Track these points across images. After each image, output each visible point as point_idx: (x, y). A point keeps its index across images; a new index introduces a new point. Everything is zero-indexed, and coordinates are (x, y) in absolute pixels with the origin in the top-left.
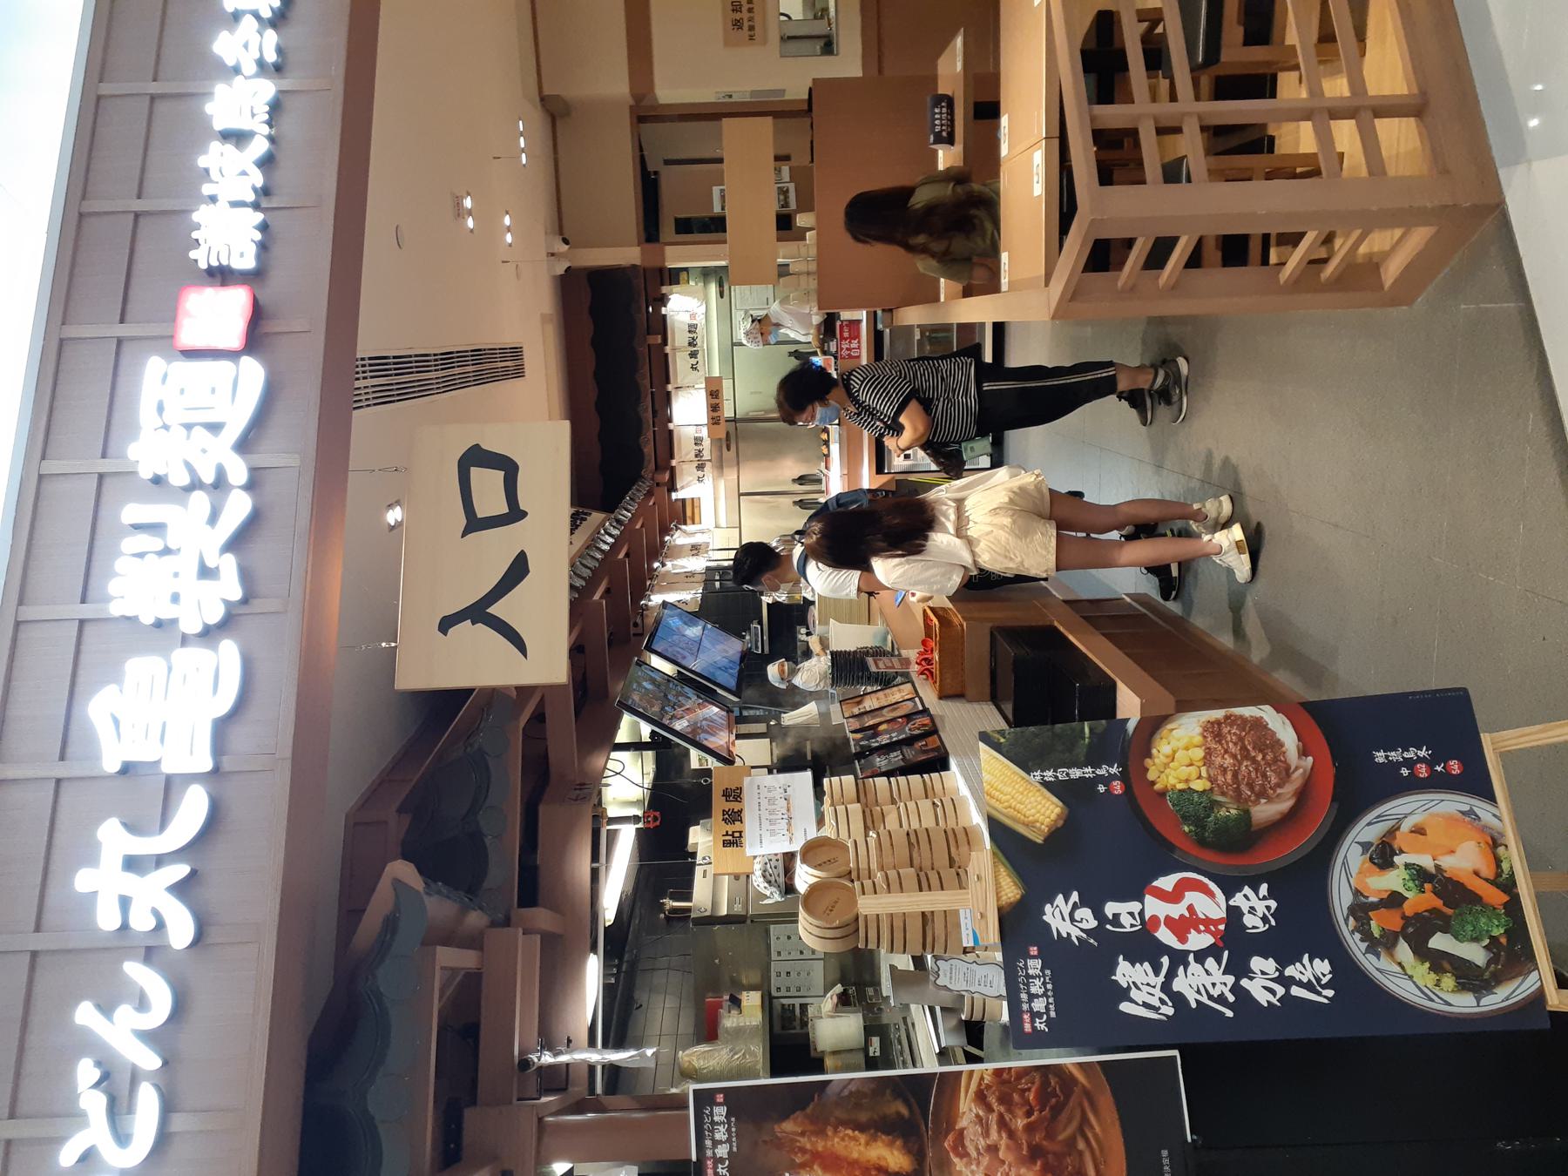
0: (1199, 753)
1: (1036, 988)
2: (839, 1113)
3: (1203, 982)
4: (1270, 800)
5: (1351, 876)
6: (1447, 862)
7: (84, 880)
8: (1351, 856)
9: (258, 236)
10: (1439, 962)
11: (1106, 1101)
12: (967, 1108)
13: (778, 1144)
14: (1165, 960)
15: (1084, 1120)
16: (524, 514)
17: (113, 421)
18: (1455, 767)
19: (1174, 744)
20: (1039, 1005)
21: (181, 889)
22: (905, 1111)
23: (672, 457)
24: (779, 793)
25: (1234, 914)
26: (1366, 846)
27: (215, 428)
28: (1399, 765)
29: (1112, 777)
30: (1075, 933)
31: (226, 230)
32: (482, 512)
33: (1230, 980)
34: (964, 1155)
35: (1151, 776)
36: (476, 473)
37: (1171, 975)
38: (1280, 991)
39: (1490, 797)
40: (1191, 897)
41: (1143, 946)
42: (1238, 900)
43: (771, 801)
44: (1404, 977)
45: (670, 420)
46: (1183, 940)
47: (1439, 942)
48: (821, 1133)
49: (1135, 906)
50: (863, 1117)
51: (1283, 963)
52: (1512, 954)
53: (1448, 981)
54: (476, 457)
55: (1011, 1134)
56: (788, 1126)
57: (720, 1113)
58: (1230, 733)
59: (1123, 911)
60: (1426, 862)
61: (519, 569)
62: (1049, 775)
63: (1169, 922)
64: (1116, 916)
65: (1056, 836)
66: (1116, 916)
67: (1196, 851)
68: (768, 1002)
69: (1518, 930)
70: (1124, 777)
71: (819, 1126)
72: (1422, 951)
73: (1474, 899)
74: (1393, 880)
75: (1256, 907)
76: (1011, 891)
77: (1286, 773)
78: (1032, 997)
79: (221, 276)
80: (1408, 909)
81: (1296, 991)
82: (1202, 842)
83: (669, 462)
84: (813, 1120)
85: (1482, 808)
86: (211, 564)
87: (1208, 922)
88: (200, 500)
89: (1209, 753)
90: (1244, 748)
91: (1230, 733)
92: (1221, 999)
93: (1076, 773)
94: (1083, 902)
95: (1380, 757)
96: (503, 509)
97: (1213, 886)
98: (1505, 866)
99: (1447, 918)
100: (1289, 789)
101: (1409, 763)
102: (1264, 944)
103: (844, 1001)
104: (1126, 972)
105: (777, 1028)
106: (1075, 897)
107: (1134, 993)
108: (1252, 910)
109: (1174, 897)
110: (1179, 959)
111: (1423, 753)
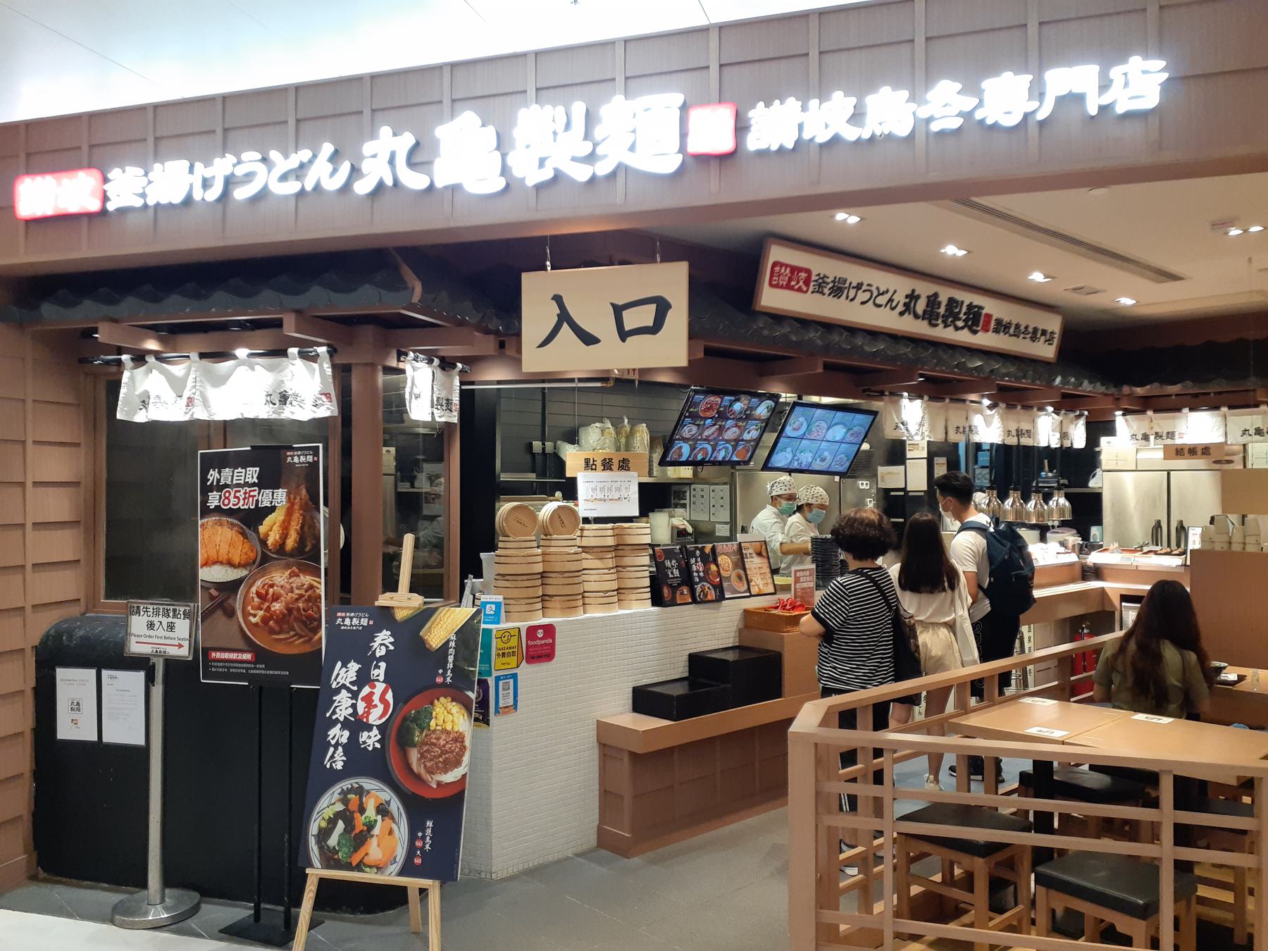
0: (449, 728)
1: (355, 621)
2: (308, 517)
3: (343, 705)
4: (419, 760)
5: (377, 792)
6: (374, 841)
7: (385, 131)
8: (386, 795)
9: (774, 148)
10: (332, 822)
11: (307, 649)
12: (307, 579)
13: (298, 486)
14: (355, 688)
15: (301, 637)
16: (623, 340)
17: (633, 82)
18: (418, 861)
19: (456, 715)
20: (347, 621)
21: (380, 186)
22: (307, 549)
23: (1156, 411)
24: (624, 493)
25: (369, 728)
26: (388, 803)
27: (632, 148)
28: (424, 832)
29: (445, 679)
30: (375, 645)
31: (777, 125)
32: (626, 314)
33: (342, 719)
34: (291, 576)
35: (442, 699)
36: (652, 308)
37: (349, 690)
38: (333, 742)
39: (401, 873)
40: (381, 707)
41: (363, 678)
42: (375, 731)
43: (618, 489)
44: (328, 804)
45: (1191, 409)
46: (363, 699)
47: (341, 825)
48: (301, 508)
49: (382, 678)
50: (306, 529)
51: (344, 746)
52: (330, 859)
53: (324, 824)
54: (663, 307)
55: (297, 600)
56: (304, 492)
57: (310, 458)
58: (456, 747)
59: (379, 672)
60: (376, 831)
61: (588, 339)
62: (452, 644)
63: (372, 694)
64: (379, 667)
65: (422, 643)
66: (379, 667)
67: (402, 713)
68: (686, 483)
69: (338, 865)
70: (444, 685)
71: (305, 508)
72: (338, 815)
73: (356, 849)
74: (371, 812)
75: (370, 739)
76: (400, 615)
77: (431, 772)
78: (351, 618)
79: (741, 128)
80: (357, 815)
81: (332, 749)
82: (405, 719)
83: (1150, 408)
84: (306, 503)
85: (395, 868)
86: (547, 163)
87: (368, 713)
88: (587, 148)
89: (448, 733)
90: (447, 752)
91: (456, 747)
92: (334, 712)
93: (451, 659)
94: (388, 651)
95: (430, 824)
96: (628, 327)
97: (384, 720)
98: (368, 869)
99: (350, 833)
100: (423, 771)
101: (423, 838)
102: (354, 738)
103: (681, 533)
104: (354, 667)
105: (674, 488)
106: (392, 648)
107: (344, 670)
108: (369, 737)
109: (383, 699)
110: (355, 695)
111: (427, 847)
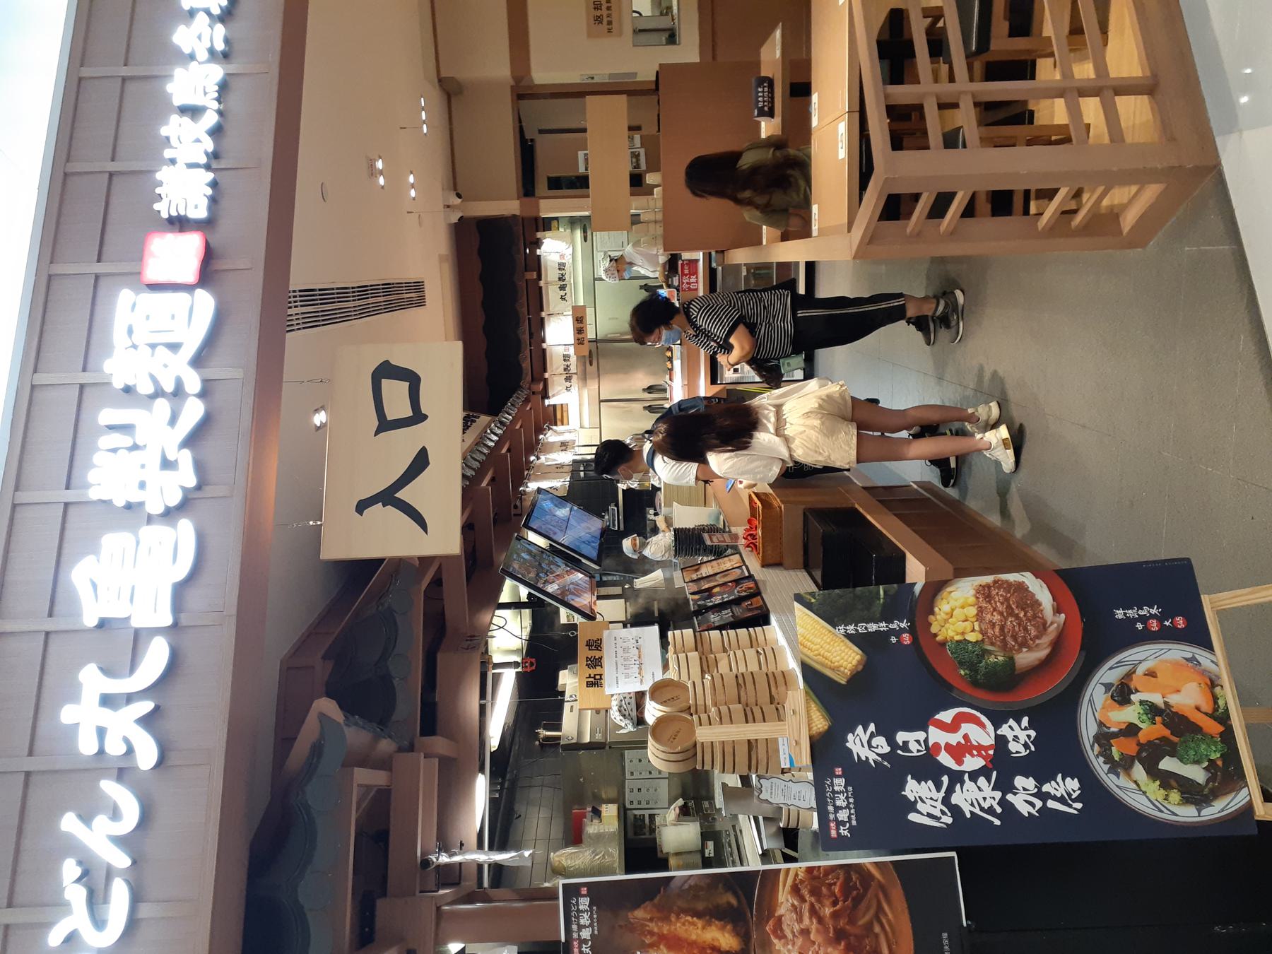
0: (973, 611)
1: (841, 801)
2: (681, 903)
3: (976, 797)
4: (1030, 649)
5: (1096, 710)
6: (1174, 699)
7: (68, 714)
8: (1096, 695)
9: (209, 192)
10: (1167, 781)
11: (897, 893)
12: (784, 899)
13: (631, 928)
14: (945, 779)
15: (880, 908)
16: (425, 417)
17: (92, 342)
18: (1180, 622)
19: (953, 603)
20: (843, 815)
21: (147, 721)
22: (734, 901)
23: (545, 370)
24: (632, 643)
25: (1001, 741)
26: (1108, 686)
27: (174, 347)
28: (1135, 621)
29: (902, 630)
30: (872, 757)
31: (183, 187)
32: (391, 415)
33: (998, 795)
34: (782, 937)
35: (934, 629)
36: (386, 384)
37: (950, 791)
38: (1039, 804)
39: (1208, 646)
40: (966, 728)
41: (927, 768)
42: (1004, 730)
43: (626, 650)
44: (1139, 793)
45: (544, 341)
46: (960, 762)
47: (1167, 764)
48: (666, 919)
49: (920, 735)
50: (700, 906)
51: (1041, 781)
52: (1227, 774)
53: (1175, 796)
54: (386, 371)
55: (820, 920)
56: (640, 914)
57: (584, 903)
58: (998, 594)
59: (911, 739)
60: (1157, 699)
61: (421, 462)
62: (851, 629)
63: (949, 748)
64: (906, 743)
65: (857, 678)
66: (906, 743)
67: (970, 691)
68: (623, 812)
69: (1231, 755)
70: (912, 630)
71: (665, 913)
72: (1153, 772)
73: (1196, 729)
74: (1130, 714)
75: (1019, 736)
76: (820, 723)
77: (1043, 627)
78: (837, 809)
79: (179, 224)
80: (1143, 737)
81: (1051, 804)
82: (975, 683)
83: (542, 375)
84: (660, 908)
85: (1202, 656)
86: (171, 457)
87: (980, 748)
88: (163, 406)
89: (981, 611)
90: (1009, 607)
91: (998, 594)
92: (991, 811)
93: (873, 627)
94: (879, 732)
95: (1119, 614)
96: (408, 413)
97: (984, 719)
98: (1221, 702)
99: (1174, 745)
100: (1046, 640)
101: (1143, 619)
102: (1025, 766)
103: (685, 812)
104: (913, 789)
105: (631, 834)
106: (872, 727)
107: (920, 806)
108: (1016, 738)
109: (952, 727)
110: (956, 778)
111: (1154, 611)
